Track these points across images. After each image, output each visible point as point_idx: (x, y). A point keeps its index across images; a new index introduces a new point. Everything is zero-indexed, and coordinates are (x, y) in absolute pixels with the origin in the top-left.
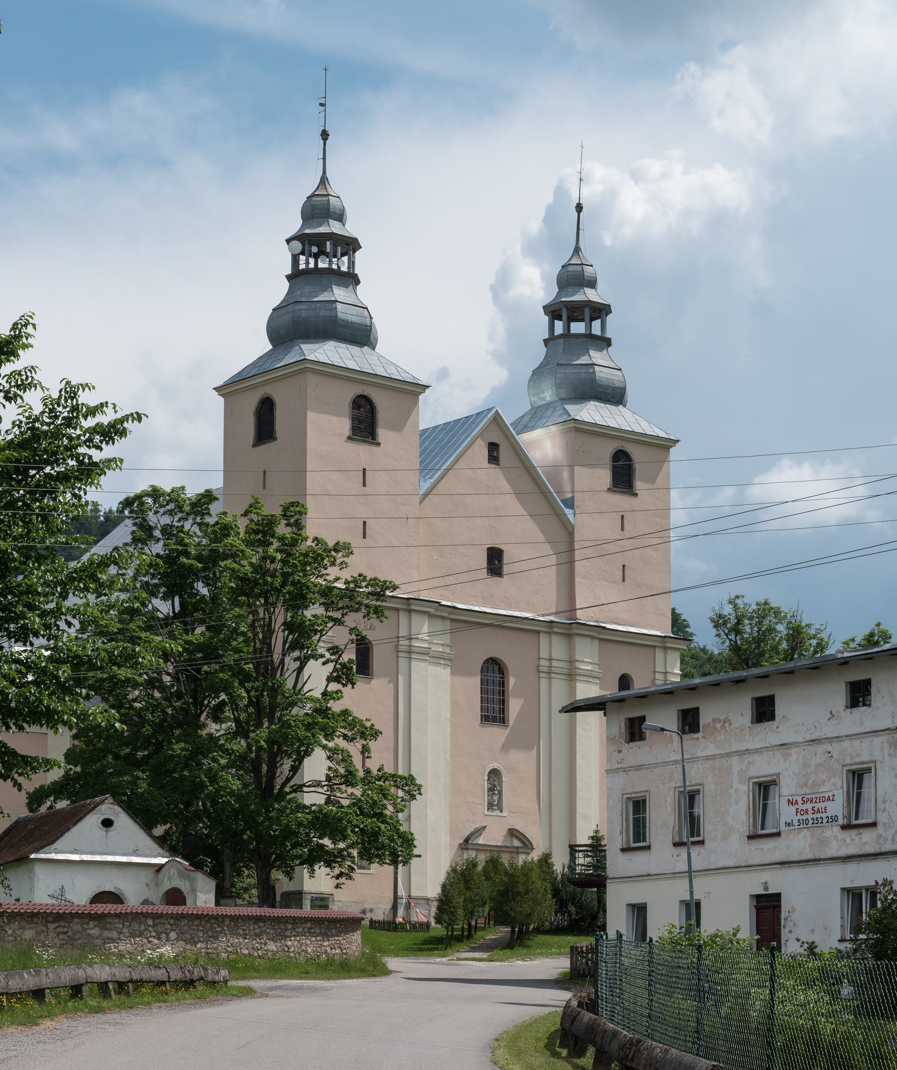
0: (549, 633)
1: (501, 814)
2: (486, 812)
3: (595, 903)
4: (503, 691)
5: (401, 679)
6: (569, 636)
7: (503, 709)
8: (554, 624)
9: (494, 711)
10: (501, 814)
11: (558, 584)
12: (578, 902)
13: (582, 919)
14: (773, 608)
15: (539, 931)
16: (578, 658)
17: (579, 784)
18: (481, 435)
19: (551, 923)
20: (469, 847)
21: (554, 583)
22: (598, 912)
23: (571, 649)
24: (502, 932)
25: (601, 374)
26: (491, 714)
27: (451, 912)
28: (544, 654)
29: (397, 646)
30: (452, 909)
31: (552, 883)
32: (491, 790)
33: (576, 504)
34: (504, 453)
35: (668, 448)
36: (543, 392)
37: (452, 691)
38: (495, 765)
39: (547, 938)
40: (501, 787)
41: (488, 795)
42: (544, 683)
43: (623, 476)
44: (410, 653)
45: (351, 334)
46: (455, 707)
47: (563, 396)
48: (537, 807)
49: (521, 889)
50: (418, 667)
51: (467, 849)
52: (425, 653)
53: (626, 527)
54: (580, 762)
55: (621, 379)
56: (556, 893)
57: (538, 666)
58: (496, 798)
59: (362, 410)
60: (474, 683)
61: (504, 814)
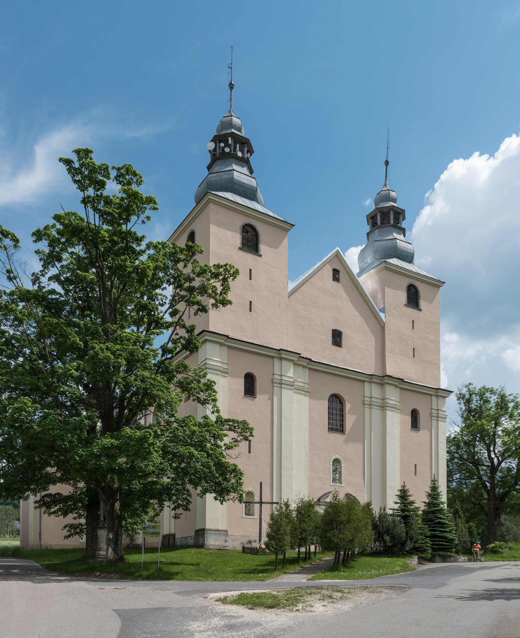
0: (370, 382)
1: (341, 485)
2: (332, 484)
3: (404, 534)
4: (342, 414)
5: (275, 399)
6: (382, 385)
7: (343, 425)
8: (373, 376)
9: (336, 424)
10: (341, 485)
11: (376, 355)
12: (391, 534)
13: (394, 546)
14: (488, 389)
15: (363, 554)
16: (387, 397)
17: (388, 469)
18: (328, 262)
19: (372, 549)
20: (320, 503)
21: (374, 354)
22: (406, 541)
23: (383, 392)
24: (329, 557)
25: (400, 244)
26: (334, 427)
27: (279, 539)
28: (367, 394)
29: (273, 379)
30: (280, 536)
31: (372, 521)
32: (335, 471)
33: (386, 310)
34: (342, 275)
35: (439, 287)
36: (367, 258)
37: (310, 411)
38: (337, 457)
39: (368, 559)
40: (341, 470)
41: (333, 474)
42: (367, 411)
43: (413, 298)
44: (281, 384)
45: (243, 191)
46: (311, 420)
47: (378, 257)
48: (363, 482)
49: (344, 518)
50: (287, 394)
51: (319, 505)
52: (291, 385)
53: (415, 327)
54: (388, 456)
55: (412, 248)
56: (375, 527)
57: (364, 401)
58: (337, 475)
59: (249, 234)
60: (325, 405)
61: (343, 485)
